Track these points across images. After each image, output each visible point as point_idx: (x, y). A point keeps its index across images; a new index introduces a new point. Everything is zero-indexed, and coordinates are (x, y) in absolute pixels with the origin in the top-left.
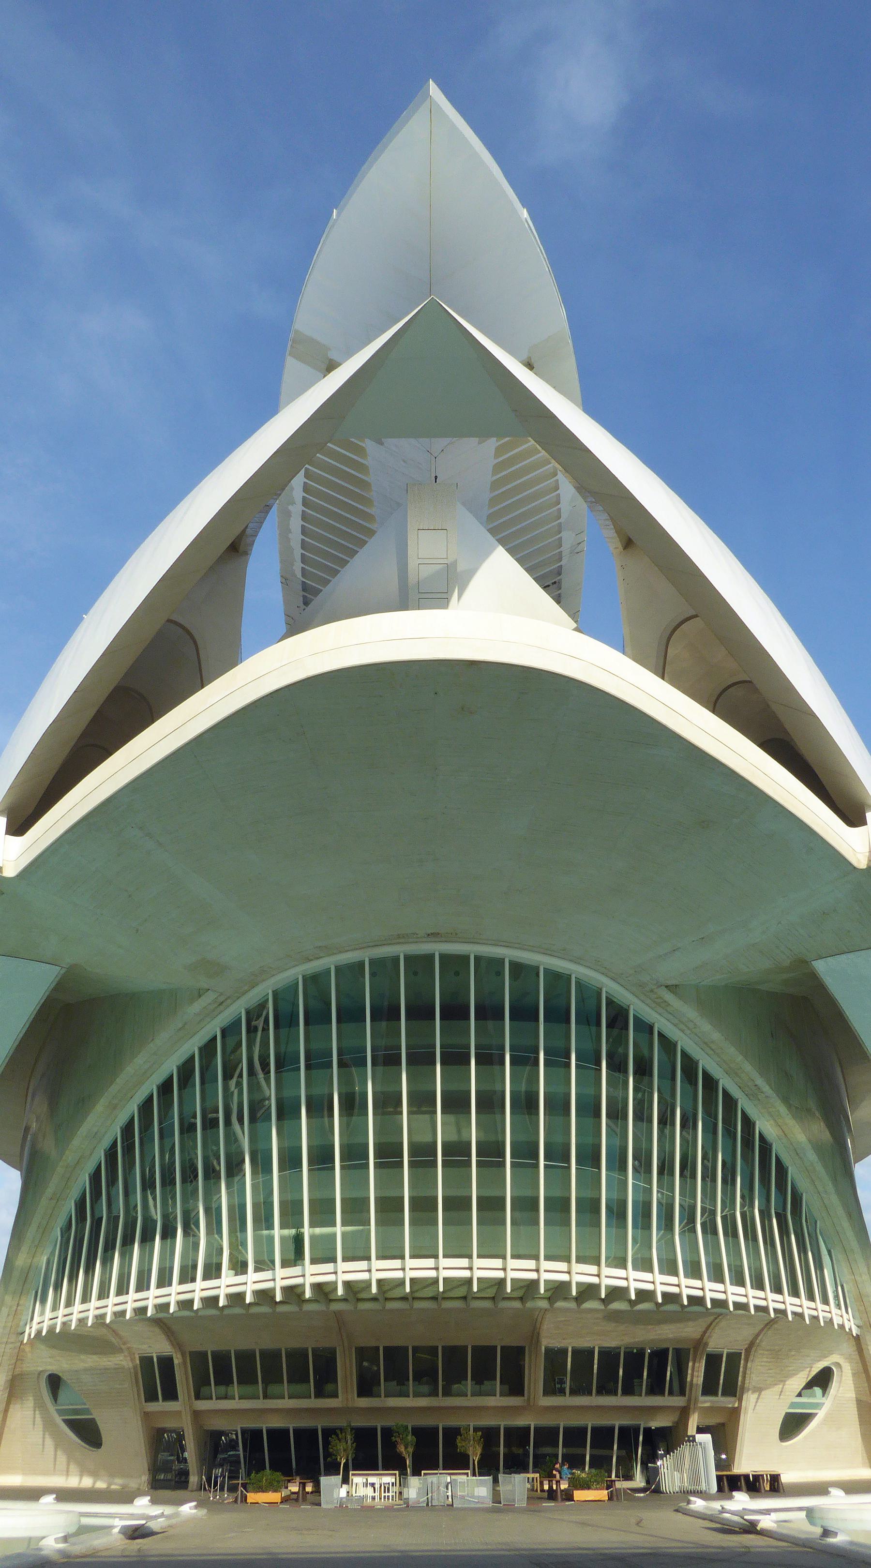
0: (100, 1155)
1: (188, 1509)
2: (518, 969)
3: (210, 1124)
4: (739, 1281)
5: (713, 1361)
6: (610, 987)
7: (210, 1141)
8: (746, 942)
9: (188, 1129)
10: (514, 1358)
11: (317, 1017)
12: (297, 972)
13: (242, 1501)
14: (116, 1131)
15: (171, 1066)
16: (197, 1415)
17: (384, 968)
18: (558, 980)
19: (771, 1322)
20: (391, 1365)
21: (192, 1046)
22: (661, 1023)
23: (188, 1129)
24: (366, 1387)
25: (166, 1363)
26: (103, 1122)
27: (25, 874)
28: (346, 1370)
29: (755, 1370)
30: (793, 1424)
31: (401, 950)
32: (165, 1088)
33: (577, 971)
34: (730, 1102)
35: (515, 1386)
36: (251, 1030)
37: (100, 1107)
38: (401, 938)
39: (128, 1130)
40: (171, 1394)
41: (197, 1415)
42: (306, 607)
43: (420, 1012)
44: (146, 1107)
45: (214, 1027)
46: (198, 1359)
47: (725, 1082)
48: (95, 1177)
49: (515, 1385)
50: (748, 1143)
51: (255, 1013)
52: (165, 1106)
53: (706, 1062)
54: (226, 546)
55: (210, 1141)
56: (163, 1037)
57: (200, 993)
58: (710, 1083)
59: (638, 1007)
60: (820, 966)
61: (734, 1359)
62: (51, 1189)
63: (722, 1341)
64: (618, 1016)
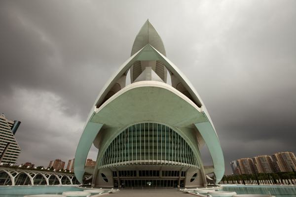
0: (108, 147)
1: (118, 190)
2: (159, 125)
3: (121, 144)
4: (185, 163)
5: (182, 172)
6: (170, 127)
7: (121, 146)
8: (188, 121)
9: (118, 144)
10: (158, 172)
11: (134, 131)
12: (132, 125)
13: (116, 172)
14: (110, 144)
15: (116, 136)
16: (120, 179)
17: (142, 124)
18: (164, 126)
19: (189, 168)
20: (143, 173)
21: (119, 134)
22: (176, 131)
23: (118, 144)
24: (140, 175)
25: (116, 172)
26: (108, 143)
27: (98, 113)
28: (138, 173)
29: (188, 173)
30: (192, 180)
31: (144, 122)
32: (116, 139)
33: (166, 125)
34: (185, 141)
35: (135, 175)
36: (126, 132)
37: (108, 141)
38: (144, 121)
39: (111, 144)
40: (116, 176)
41: (120, 179)
42: (134, 80)
43: (147, 130)
44: (113, 141)
45: (122, 132)
46: (140, 172)
47: (184, 139)
48: (107, 150)
49: (158, 175)
50: (187, 146)
51: (127, 130)
52: (113, 144)
53: (182, 136)
54: (123, 74)
55: (121, 146)
56: (115, 133)
57: (120, 127)
58: (182, 139)
59: (174, 129)
60: (196, 125)
61: (185, 172)
62: (102, 151)
63: (184, 170)
64: (171, 130)
